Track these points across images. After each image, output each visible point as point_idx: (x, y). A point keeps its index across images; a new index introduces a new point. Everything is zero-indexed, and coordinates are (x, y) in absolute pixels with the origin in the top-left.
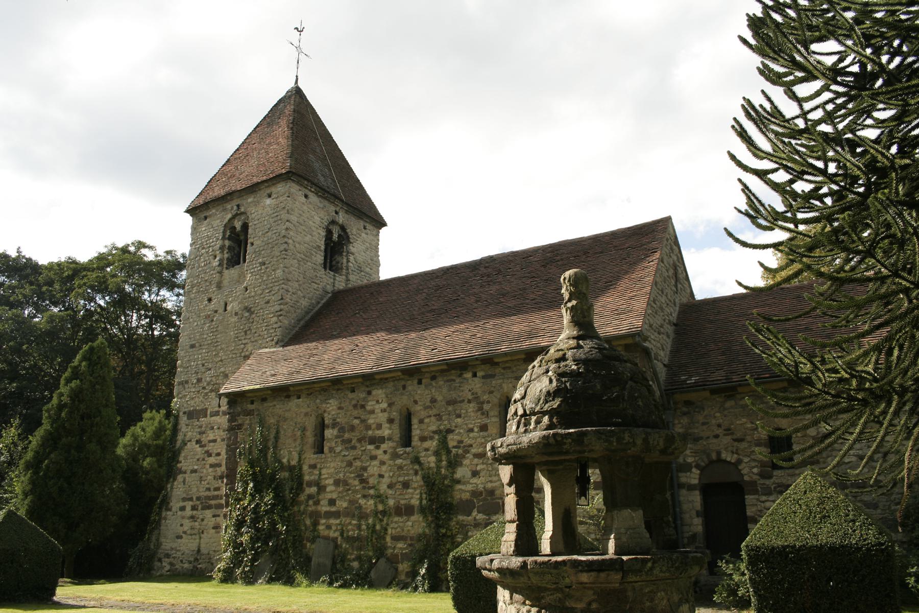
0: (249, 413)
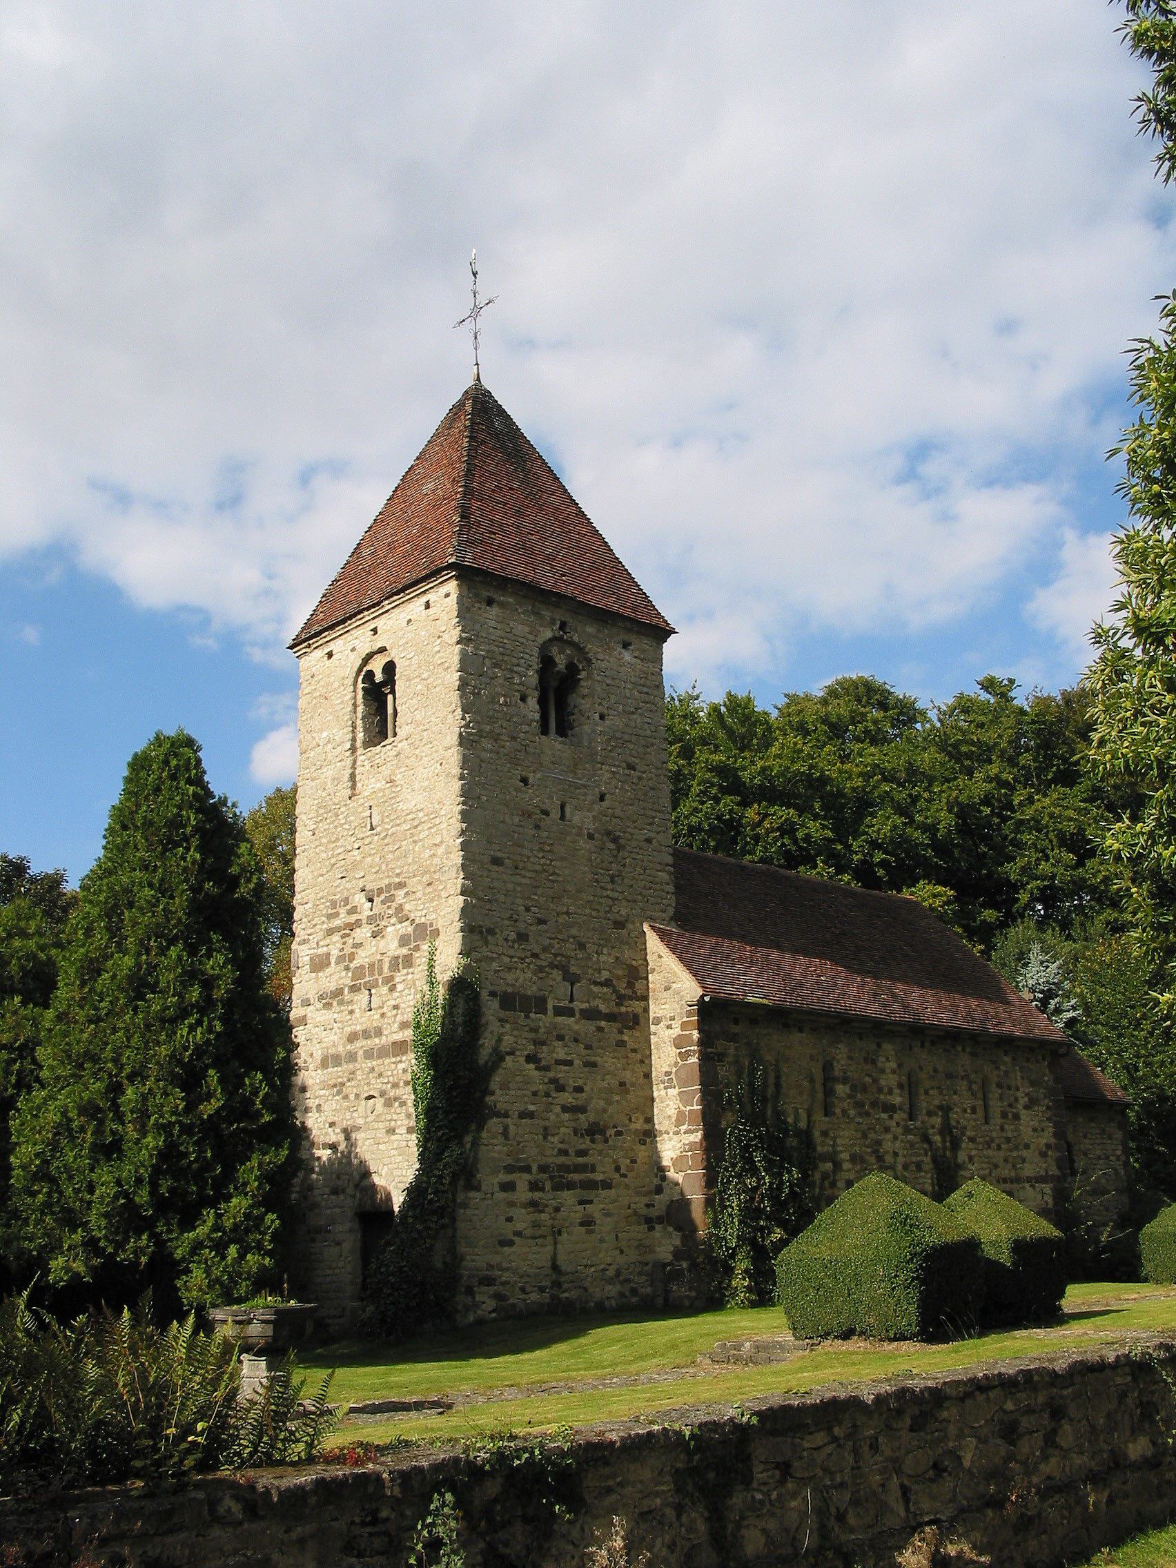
0: (733, 1038)
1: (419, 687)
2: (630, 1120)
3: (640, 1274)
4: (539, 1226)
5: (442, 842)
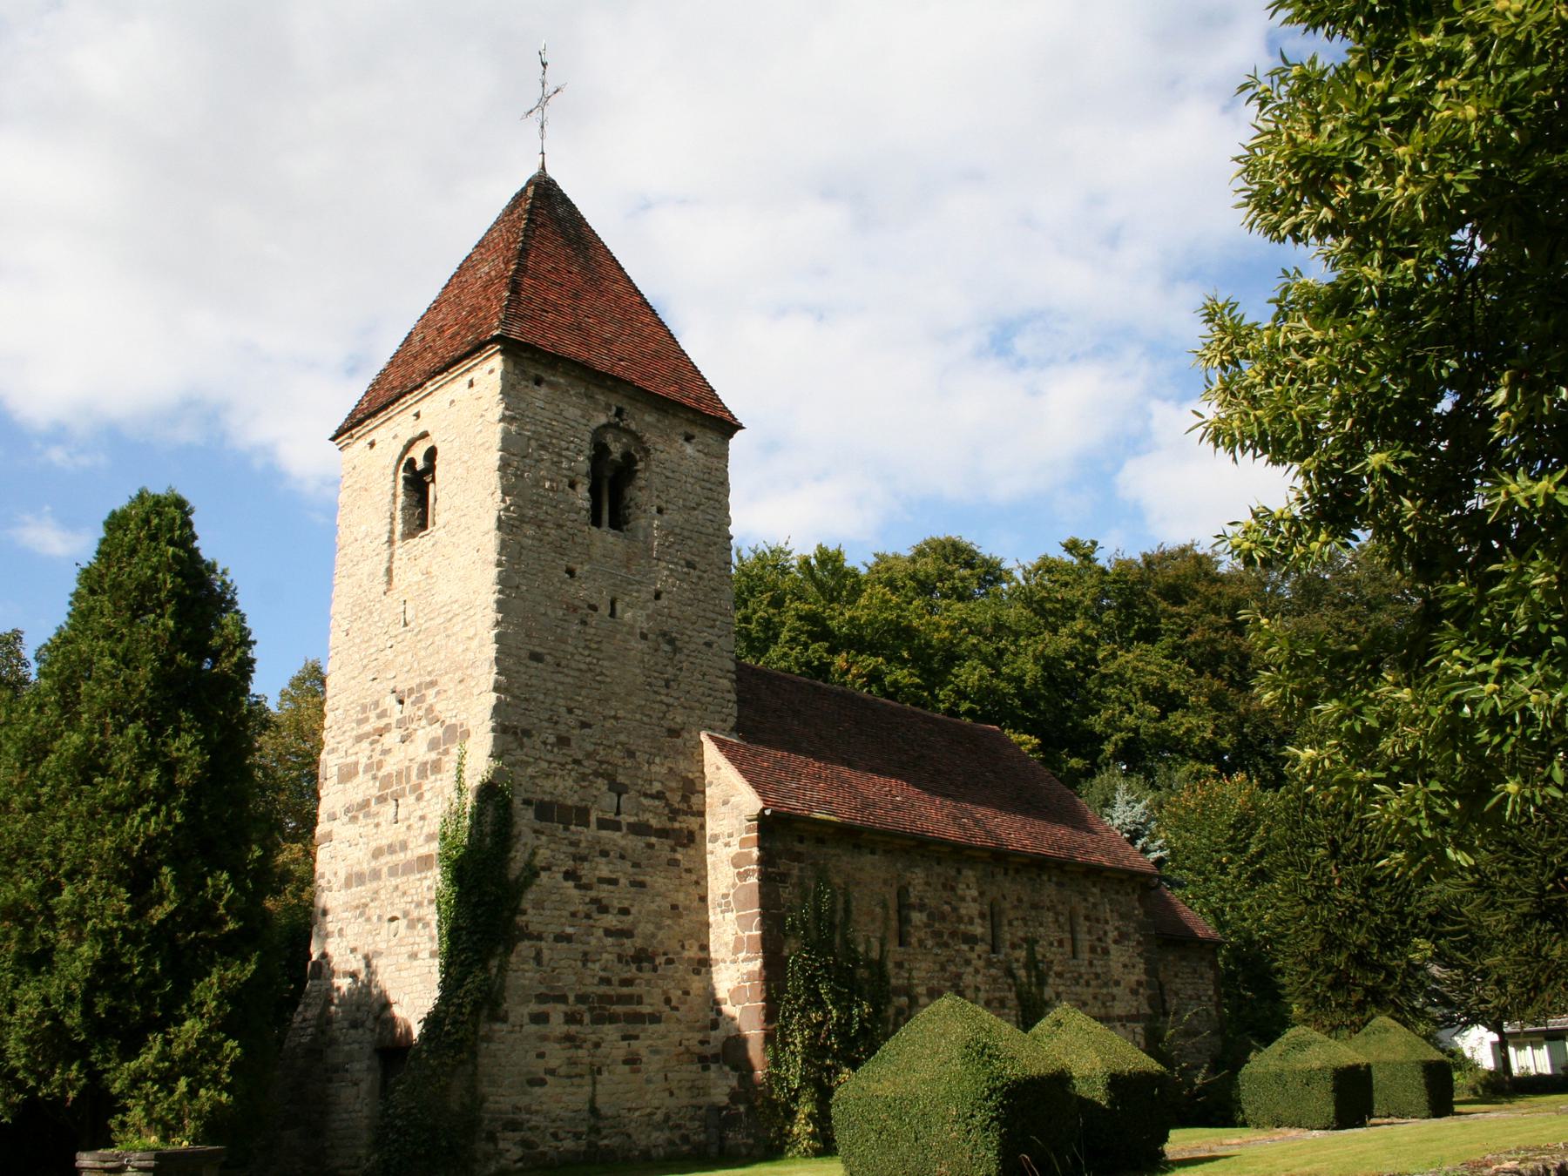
0: (798, 857)
2: (683, 947)
3: (692, 1119)
4: (575, 1063)
5: (475, 635)
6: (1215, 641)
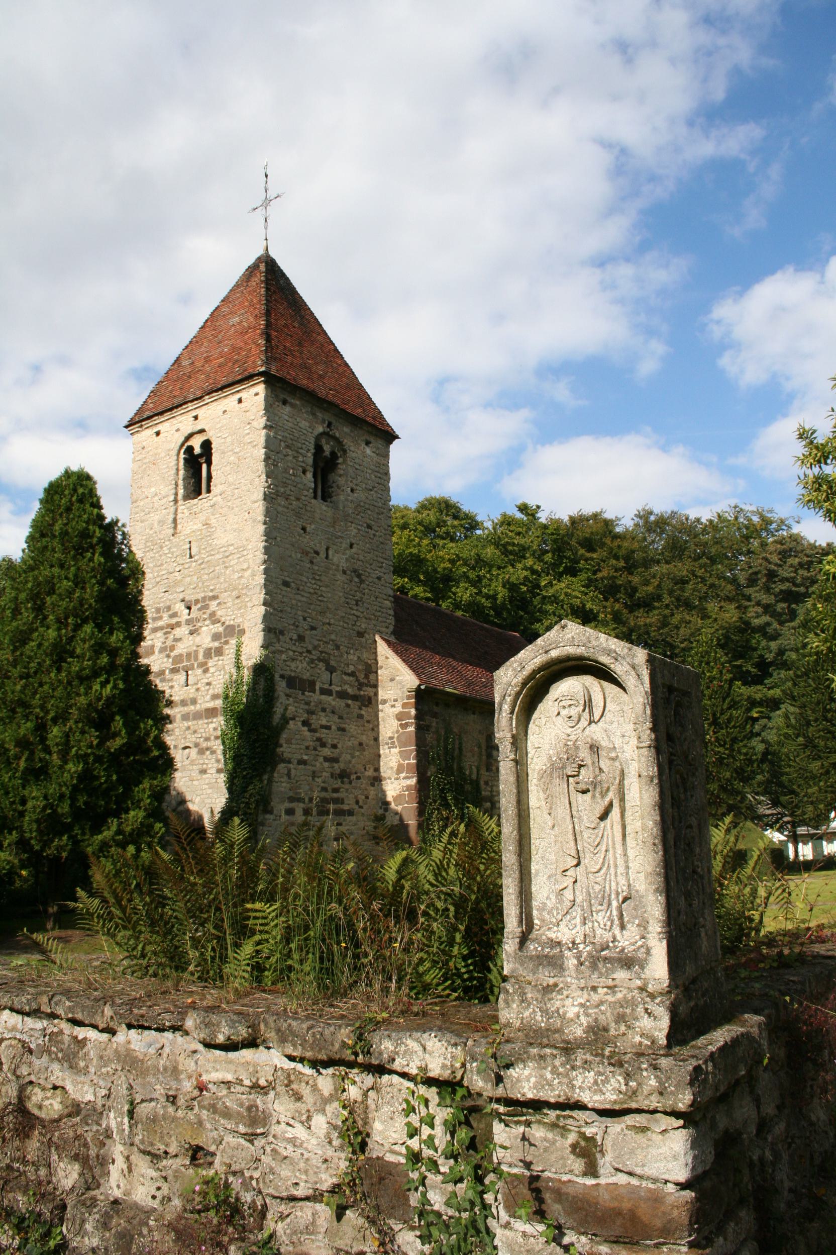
0: (435, 715)
1: (232, 458)
2: (365, 769)
5: (248, 568)
6: (616, 577)
